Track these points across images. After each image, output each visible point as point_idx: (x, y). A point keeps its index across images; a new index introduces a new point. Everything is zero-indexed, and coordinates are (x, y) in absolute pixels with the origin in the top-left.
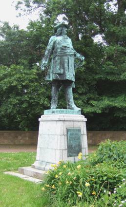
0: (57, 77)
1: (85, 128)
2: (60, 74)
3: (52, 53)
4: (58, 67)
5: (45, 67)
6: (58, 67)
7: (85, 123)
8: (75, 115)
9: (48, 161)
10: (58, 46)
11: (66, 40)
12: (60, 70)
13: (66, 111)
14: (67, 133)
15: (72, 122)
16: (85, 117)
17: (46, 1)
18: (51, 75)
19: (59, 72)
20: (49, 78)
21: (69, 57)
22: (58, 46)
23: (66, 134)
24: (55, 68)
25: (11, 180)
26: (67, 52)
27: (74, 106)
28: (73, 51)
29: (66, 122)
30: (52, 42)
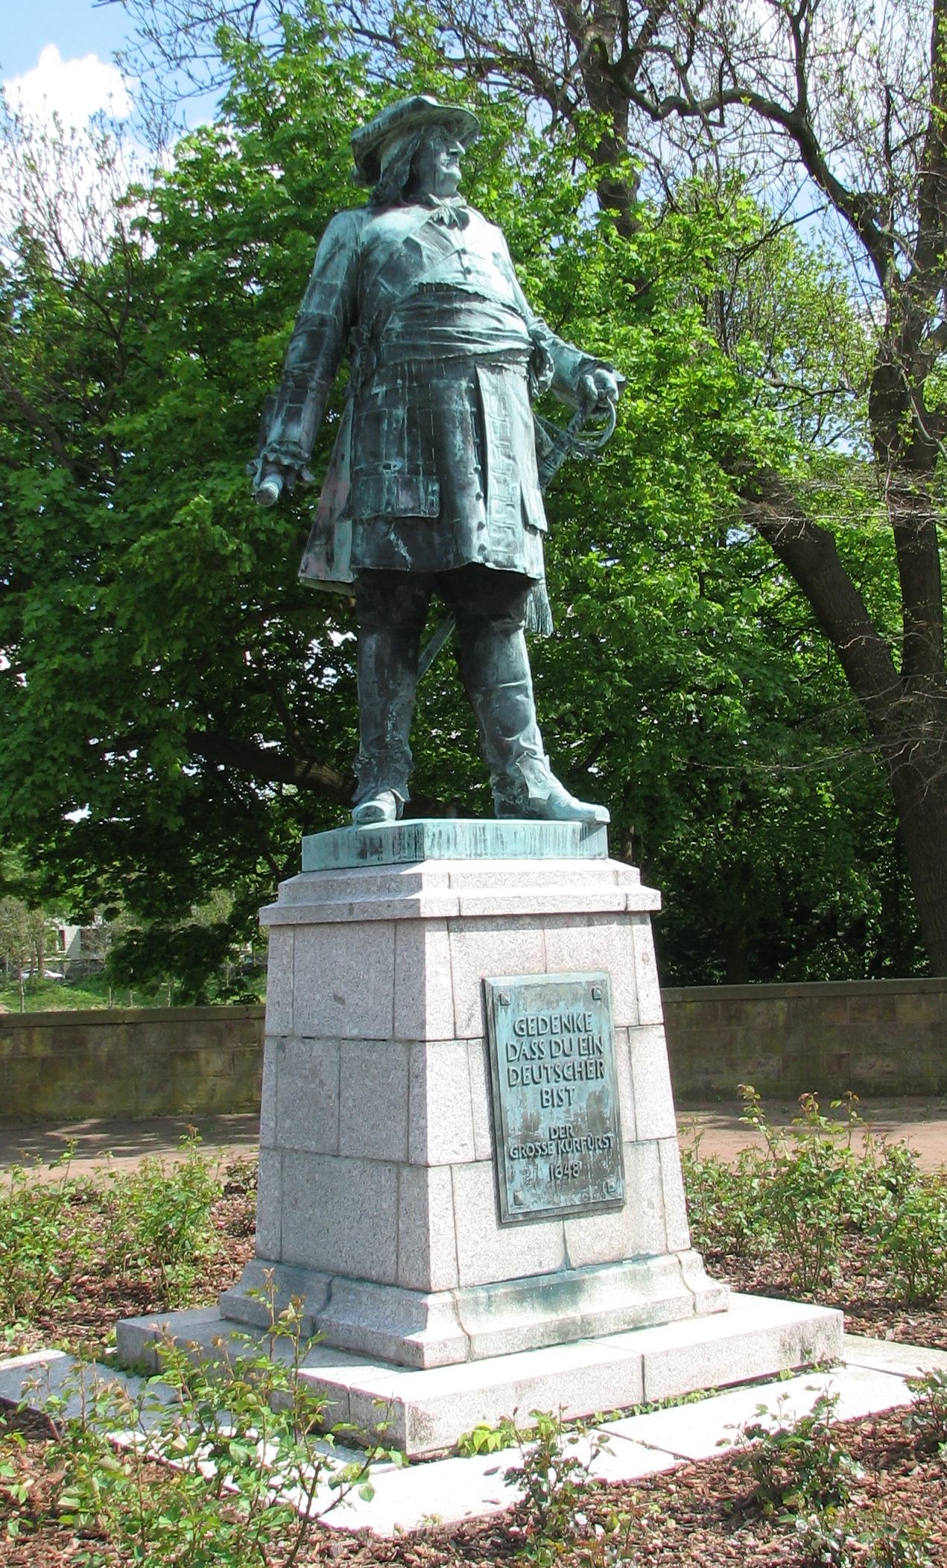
0: (387, 551)
1: (649, 973)
2: (406, 525)
3: (341, 354)
4: (397, 464)
5: (285, 471)
6: (397, 464)
7: (643, 935)
8: (552, 865)
9: (349, 1267)
10: (386, 288)
11: (455, 236)
12: (408, 485)
13: (479, 839)
14: (489, 1022)
15: (532, 937)
16: (647, 881)
17: (8, 1472)
18: (344, 531)
19: (404, 500)
20: (330, 559)
21: (483, 375)
22: (386, 288)
23: (477, 1028)
24: (366, 476)
25: (14, 1082)
26: (469, 337)
27: (542, 781)
28: (512, 323)
29: (473, 937)
30: (343, 261)
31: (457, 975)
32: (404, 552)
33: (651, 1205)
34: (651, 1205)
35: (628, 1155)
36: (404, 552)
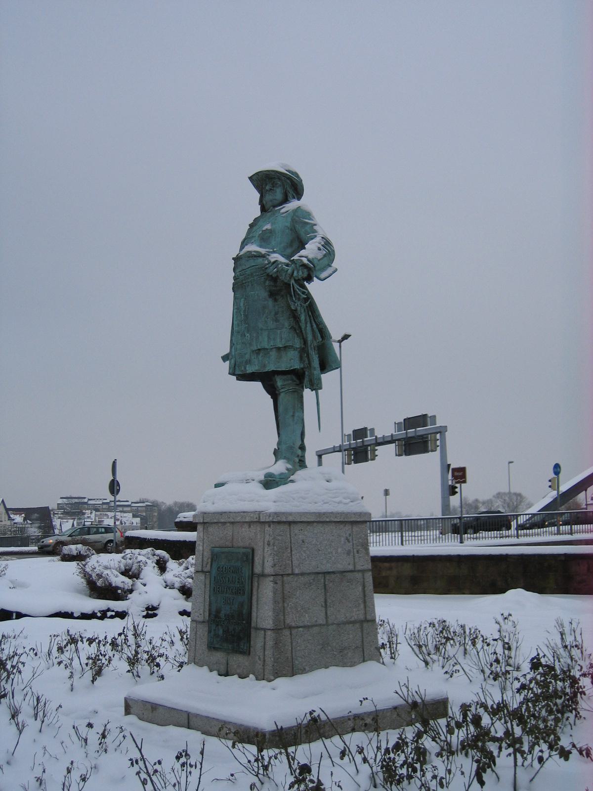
33: (259, 659)
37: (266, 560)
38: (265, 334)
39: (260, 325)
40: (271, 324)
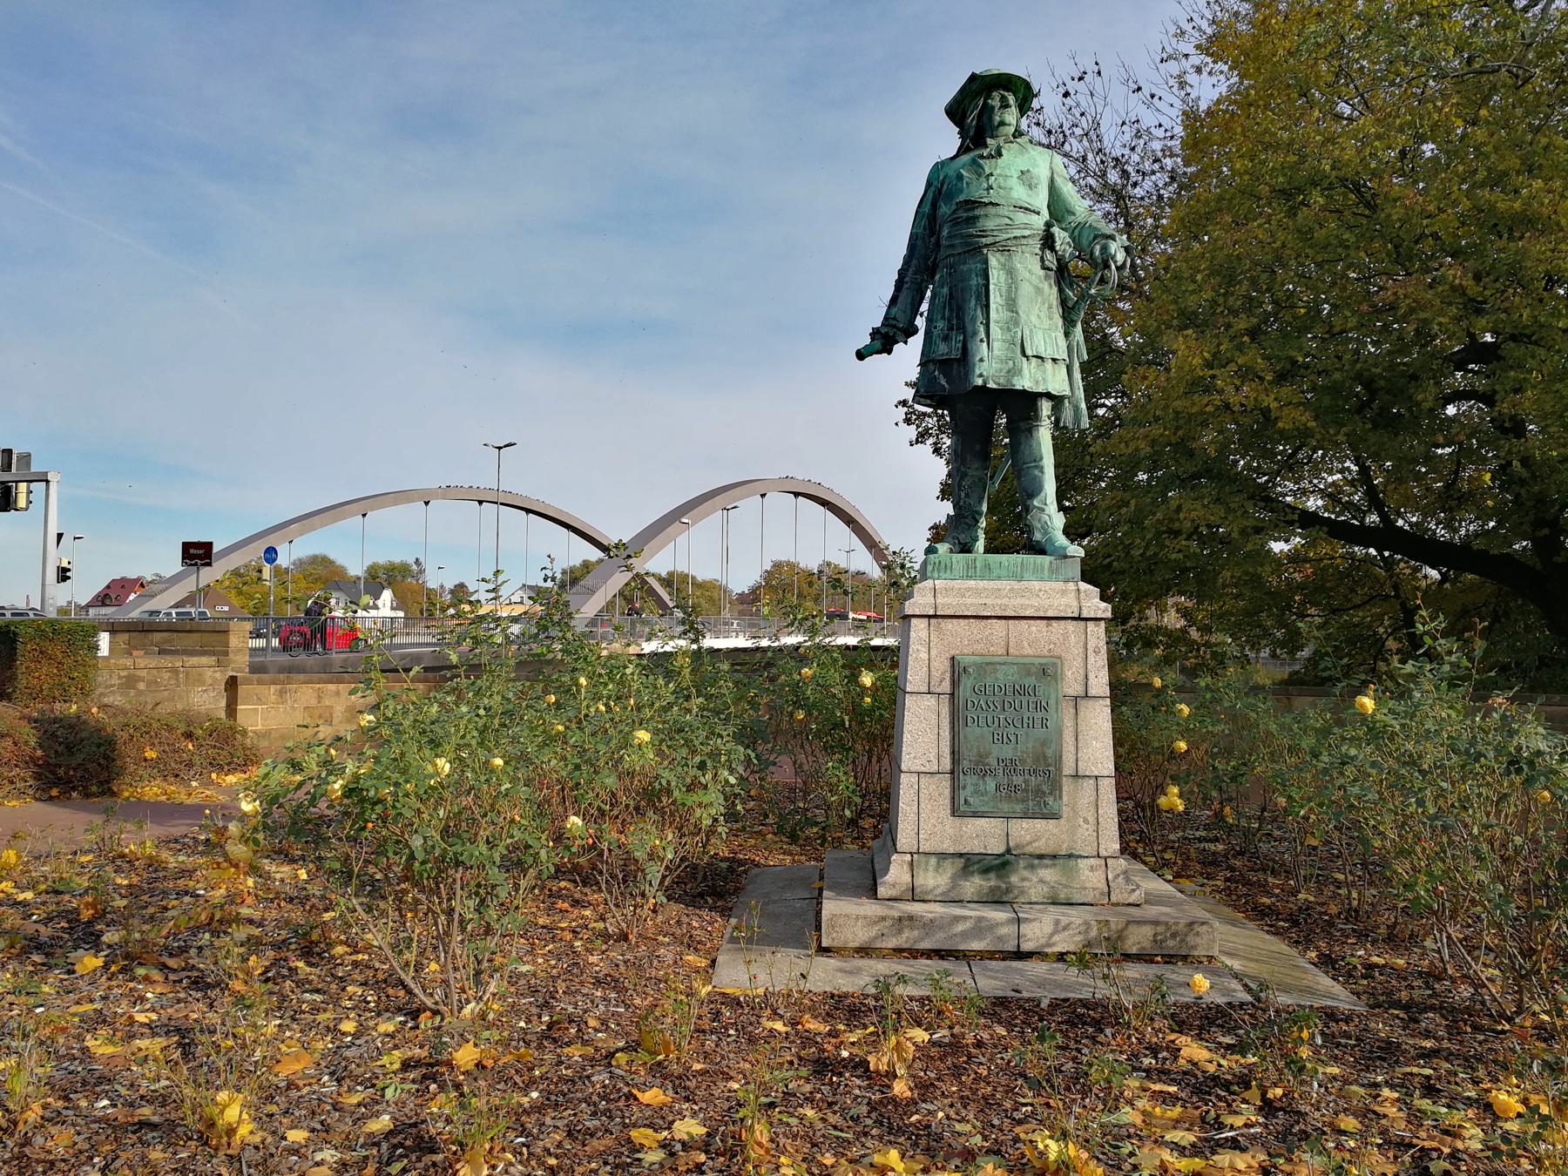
23: (946, 687)
31: (933, 652)
32: (943, 382)
33: (1086, 821)
34: (1086, 821)
35: (1067, 785)
36: (943, 382)
37: (1091, 676)
38: (1040, 334)
39: (1034, 319)
40: (1046, 324)
